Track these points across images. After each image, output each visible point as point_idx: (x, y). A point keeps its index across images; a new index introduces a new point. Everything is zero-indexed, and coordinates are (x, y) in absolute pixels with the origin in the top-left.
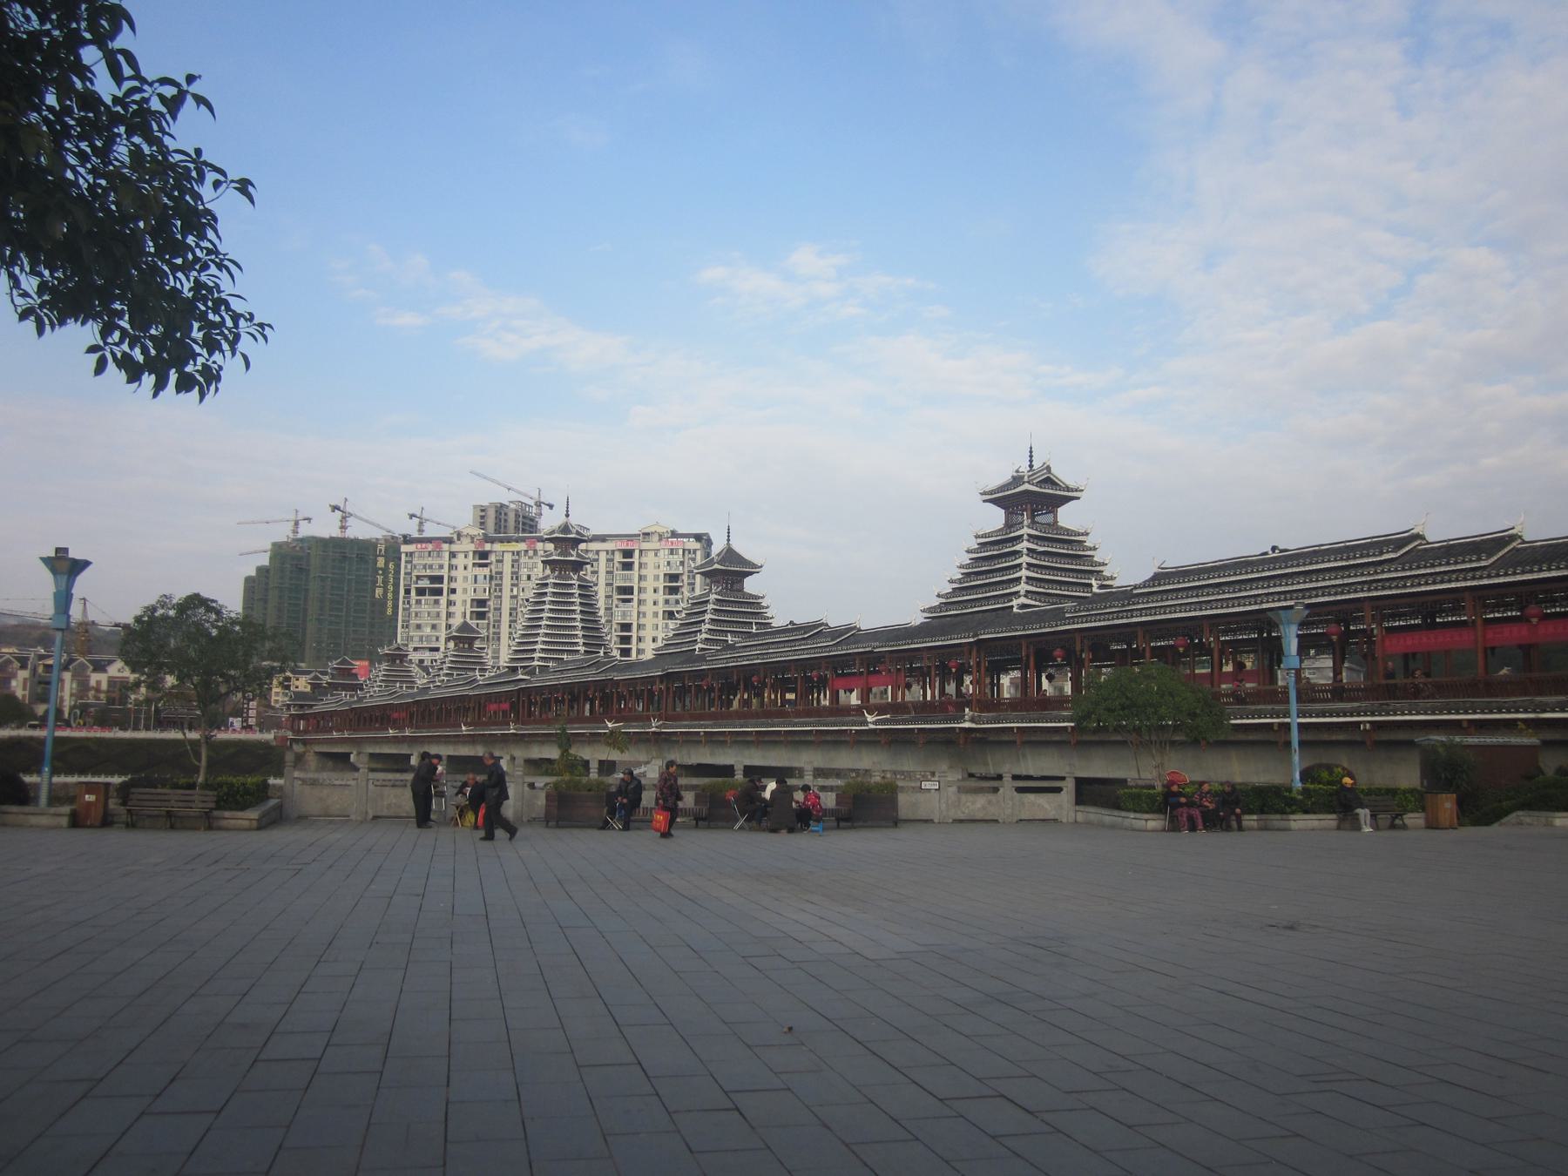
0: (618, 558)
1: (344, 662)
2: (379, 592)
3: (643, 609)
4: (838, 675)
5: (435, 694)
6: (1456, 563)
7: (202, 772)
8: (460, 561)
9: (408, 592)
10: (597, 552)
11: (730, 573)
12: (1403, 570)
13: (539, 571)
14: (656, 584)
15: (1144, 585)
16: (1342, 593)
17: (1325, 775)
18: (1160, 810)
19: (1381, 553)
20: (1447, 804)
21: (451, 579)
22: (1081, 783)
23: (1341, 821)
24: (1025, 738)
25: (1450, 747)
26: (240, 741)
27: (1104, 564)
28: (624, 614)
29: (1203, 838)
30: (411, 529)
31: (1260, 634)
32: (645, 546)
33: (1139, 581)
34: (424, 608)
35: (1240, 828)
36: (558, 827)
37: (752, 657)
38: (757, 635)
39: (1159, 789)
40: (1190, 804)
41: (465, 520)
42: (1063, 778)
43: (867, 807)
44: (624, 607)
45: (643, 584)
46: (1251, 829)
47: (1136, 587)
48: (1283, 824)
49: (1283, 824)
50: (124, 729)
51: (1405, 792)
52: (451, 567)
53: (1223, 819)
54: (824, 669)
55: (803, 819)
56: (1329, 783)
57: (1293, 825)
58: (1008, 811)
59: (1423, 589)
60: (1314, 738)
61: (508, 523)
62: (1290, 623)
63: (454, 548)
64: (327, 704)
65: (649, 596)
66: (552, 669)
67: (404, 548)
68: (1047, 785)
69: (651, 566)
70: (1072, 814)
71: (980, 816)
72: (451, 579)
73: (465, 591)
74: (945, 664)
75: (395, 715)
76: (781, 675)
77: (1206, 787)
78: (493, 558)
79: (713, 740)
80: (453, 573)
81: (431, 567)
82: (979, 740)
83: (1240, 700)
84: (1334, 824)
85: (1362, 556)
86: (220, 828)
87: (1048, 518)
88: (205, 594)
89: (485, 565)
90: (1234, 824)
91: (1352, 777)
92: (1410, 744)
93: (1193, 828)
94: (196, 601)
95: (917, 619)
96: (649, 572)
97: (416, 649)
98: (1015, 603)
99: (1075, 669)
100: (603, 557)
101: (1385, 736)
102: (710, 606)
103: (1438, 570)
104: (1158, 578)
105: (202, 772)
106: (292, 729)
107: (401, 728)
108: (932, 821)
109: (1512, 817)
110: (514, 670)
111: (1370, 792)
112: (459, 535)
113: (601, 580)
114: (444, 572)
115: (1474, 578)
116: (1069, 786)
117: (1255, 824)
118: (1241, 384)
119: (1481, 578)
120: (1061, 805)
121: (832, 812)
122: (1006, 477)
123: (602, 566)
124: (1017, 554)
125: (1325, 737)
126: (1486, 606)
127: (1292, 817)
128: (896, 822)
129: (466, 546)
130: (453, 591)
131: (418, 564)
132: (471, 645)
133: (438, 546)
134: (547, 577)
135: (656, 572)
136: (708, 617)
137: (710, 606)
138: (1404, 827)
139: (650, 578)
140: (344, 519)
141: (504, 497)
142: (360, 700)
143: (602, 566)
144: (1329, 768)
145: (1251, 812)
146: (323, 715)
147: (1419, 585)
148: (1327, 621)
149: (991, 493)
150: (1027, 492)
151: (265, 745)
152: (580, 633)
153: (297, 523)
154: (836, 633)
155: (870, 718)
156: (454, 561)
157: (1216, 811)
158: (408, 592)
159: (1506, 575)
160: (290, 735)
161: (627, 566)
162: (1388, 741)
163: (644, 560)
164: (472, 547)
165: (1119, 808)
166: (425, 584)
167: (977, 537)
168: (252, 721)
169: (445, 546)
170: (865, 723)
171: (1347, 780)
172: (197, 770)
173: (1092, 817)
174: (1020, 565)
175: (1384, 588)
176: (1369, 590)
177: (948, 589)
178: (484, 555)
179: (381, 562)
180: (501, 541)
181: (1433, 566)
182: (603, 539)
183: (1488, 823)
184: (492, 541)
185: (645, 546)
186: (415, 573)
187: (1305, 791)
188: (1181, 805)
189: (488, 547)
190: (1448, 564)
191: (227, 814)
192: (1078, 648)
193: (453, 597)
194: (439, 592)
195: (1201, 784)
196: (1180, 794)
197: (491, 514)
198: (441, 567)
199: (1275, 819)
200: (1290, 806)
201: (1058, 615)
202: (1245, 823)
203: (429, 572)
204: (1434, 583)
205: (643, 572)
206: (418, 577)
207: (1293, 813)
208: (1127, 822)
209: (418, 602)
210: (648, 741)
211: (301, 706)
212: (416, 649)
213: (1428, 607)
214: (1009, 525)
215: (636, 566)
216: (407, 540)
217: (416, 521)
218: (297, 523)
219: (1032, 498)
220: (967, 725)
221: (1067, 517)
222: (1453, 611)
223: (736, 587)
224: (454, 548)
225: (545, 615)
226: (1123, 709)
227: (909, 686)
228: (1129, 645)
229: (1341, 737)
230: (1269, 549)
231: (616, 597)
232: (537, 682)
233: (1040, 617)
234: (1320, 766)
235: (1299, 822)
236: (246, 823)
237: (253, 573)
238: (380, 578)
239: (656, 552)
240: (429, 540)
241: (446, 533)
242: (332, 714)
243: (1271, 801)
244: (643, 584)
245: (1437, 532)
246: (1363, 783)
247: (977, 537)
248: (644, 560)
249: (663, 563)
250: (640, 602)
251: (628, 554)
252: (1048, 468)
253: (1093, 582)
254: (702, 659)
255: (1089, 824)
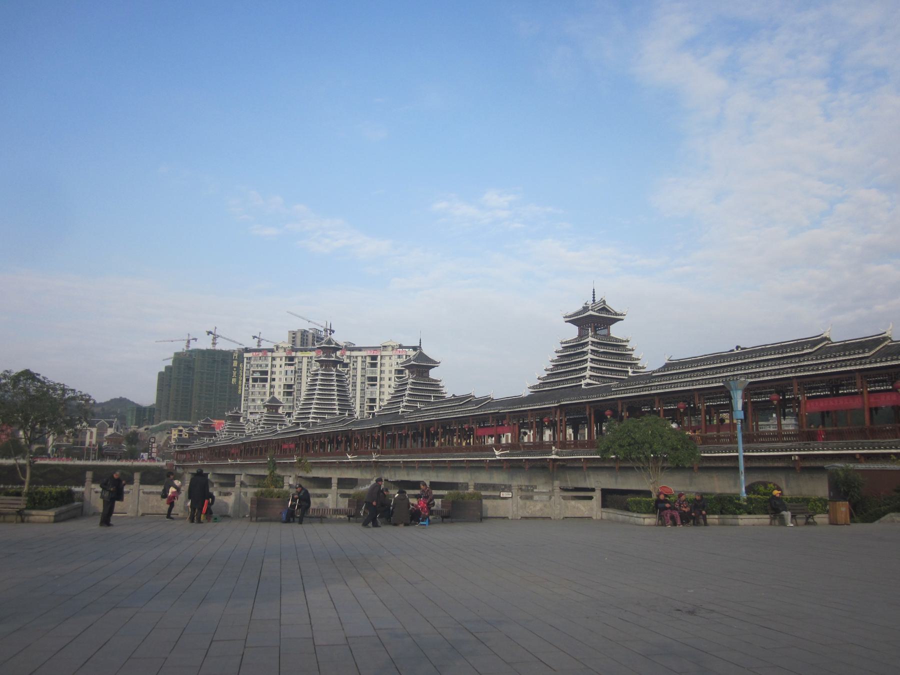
0: (368, 360)
1: (207, 420)
2: (234, 380)
3: (382, 390)
4: (480, 427)
5: (254, 439)
6: (850, 355)
7: (26, 484)
8: (277, 362)
9: (247, 380)
10: (357, 357)
11: (420, 366)
12: (817, 359)
13: (315, 367)
14: (390, 376)
15: (659, 371)
16: (779, 374)
17: (762, 488)
18: (653, 512)
19: (803, 349)
20: (843, 508)
21: (272, 373)
22: (605, 492)
23: (772, 519)
24: (589, 465)
25: (847, 471)
26: (146, 467)
27: (638, 359)
28: (372, 393)
29: (682, 531)
30: (253, 345)
31: (831, 391)
32: (384, 353)
33: (656, 368)
34: (257, 389)
35: (706, 524)
36: (257, 521)
37: (430, 416)
38: (434, 403)
39: (654, 497)
40: (673, 508)
41: (284, 340)
42: (593, 490)
43: (461, 509)
44: (371, 389)
45: (383, 375)
46: (714, 524)
47: (654, 372)
48: (734, 521)
49: (734, 521)
50: (79, 459)
51: (815, 501)
52: (272, 366)
53: (694, 518)
54: (473, 425)
55: (414, 517)
56: (765, 494)
57: (740, 522)
58: (557, 512)
59: (829, 371)
60: (754, 466)
61: (303, 340)
62: (736, 389)
63: (274, 355)
64: (196, 445)
65: (386, 382)
66: (317, 423)
67: (246, 355)
68: (583, 493)
69: (387, 365)
70: (599, 514)
71: (538, 515)
72: (272, 373)
73: (280, 379)
74: (541, 420)
75: (233, 451)
76: (446, 427)
77: (683, 498)
78: (296, 360)
79: (408, 466)
80: (274, 369)
81: (261, 366)
82: (562, 467)
83: (705, 440)
84: (768, 521)
85: (791, 351)
86: (28, 522)
87: (604, 332)
88: (34, 370)
89: (292, 365)
90: (702, 521)
91: (779, 489)
92: (821, 469)
93: (675, 524)
94: (28, 375)
95: (525, 393)
96: (386, 368)
97: (251, 413)
98: (583, 382)
99: (614, 421)
100: (360, 359)
101: (807, 464)
102: (409, 386)
103: (838, 359)
104: (667, 366)
105: (26, 484)
106: (177, 460)
107: (235, 459)
108: (507, 518)
109: (887, 517)
110: (298, 424)
111: (792, 500)
112: (277, 347)
113: (358, 373)
114: (269, 369)
115: (861, 364)
116: (597, 495)
117: (717, 521)
118: (719, 250)
119: (865, 363)
120: (592, 508)
121: (438, 512)
122: (579, 307)
123: (359, 365)
124: (585, 353)
125: (770, 464)
126: (869, 382)
127: (740, 516)
128: (482, 518)
129: (281, 353)
130: (274, 380)
131: (254, 363)
132: (277, 411)
133: (265, 353)
134: (317, 370)
135: (390, 368)
136: (407, 392)
137: (409, 386)
138: (815, 524)
139: (387, 372)
140: (214, 339)
141: (306, 326)
142: (214, 442)
143: (359, 365)
144: (765, 484)
145: (714, 513)
146: (194, 451)
147: (827, 368)
148: (771, 393)
149: (570, 317)
150: (591, 316)
151: (161, 469)
152: (337, 403)
153: (189, 342)
154: (479, 401)
155: (497, 453)
156: (274, 363)
157: (690, 513)
158: (247, 380)
159: (881, 361)
160: (175, 463)
161: (374, 365)
162: (809, 467)
163: (383, 361)
164: (284, 354)
165: (628, 510)
166: (257, 375)
167: (562, 343)
168: (154, 455)
169: (269, 354)
170: (495, 456)
171: (776, 492)
172: (23, 483)
173: (612, 516)
174: (586, 360)
175: (805, 371)
176: (796, 372)
177: (545, 374)
178: (291, 359)
179: (235, 364)
180: (301, 350)
181: (835, 356)
182: (360, 349)
183: (872, 521)
184: (296, 350)
185: (384, 353)
186: (252, 369)
187: (749, 500)
188: (666, 509)
189: (293, 354)
190: (845, 355)
191: (34, 512)
192: (620, 409)
193: (273, 383)
194: (265, 380)
195: (680, 495)
196: (665, 501)
197: (299, 336)
198: (267, 366)
199: (729, 518)
200: (739, 509)
201: (608, 390)
202: (709, 521)
203: (259, 369)
204: (836, 367)
205: (383, 368)
206: (254, 372)
207: (741, 514)
208: (632, 520)
209: (254, 386)
210: (371, 466)
211: (182, 446)
212: (251, 413)
213: (834, 383)
214: (581, 335)
215: (379, 365)
216: (247, 350)
217: (256, 340)
218: (189, 342)
219: (595, 320)
220: (554, 457)
221: (615, 331)
222: (848, 386)
223: (425, 375)
224: (274, 355)
225: (316, 392)
226: (630, 445)
227: (37, 391)
228: (652, 408)
229: (780, 465)
230: (734, 348)
231: (367, 383)
232: (310, 431)
233: (597, 391)
234: (759, 483)
235: (745, 520)
236: (46, 518)
237: (163, 370)
238: (235, 373)
239: (390, 357)
240: (260, 350)
241: (271, 346)
242: (199, 450)
243: (726, 505)
244: (383, 375)
245: (837, 337)
246: (787, 493)
247: (562, 343)
248: (383, 361)
249: (394, 363)
250: (381, 386)
251: (374, 358)
252: (604, 302)
253: (629, 369)
254: (402, 417)
255: (610, 520)
